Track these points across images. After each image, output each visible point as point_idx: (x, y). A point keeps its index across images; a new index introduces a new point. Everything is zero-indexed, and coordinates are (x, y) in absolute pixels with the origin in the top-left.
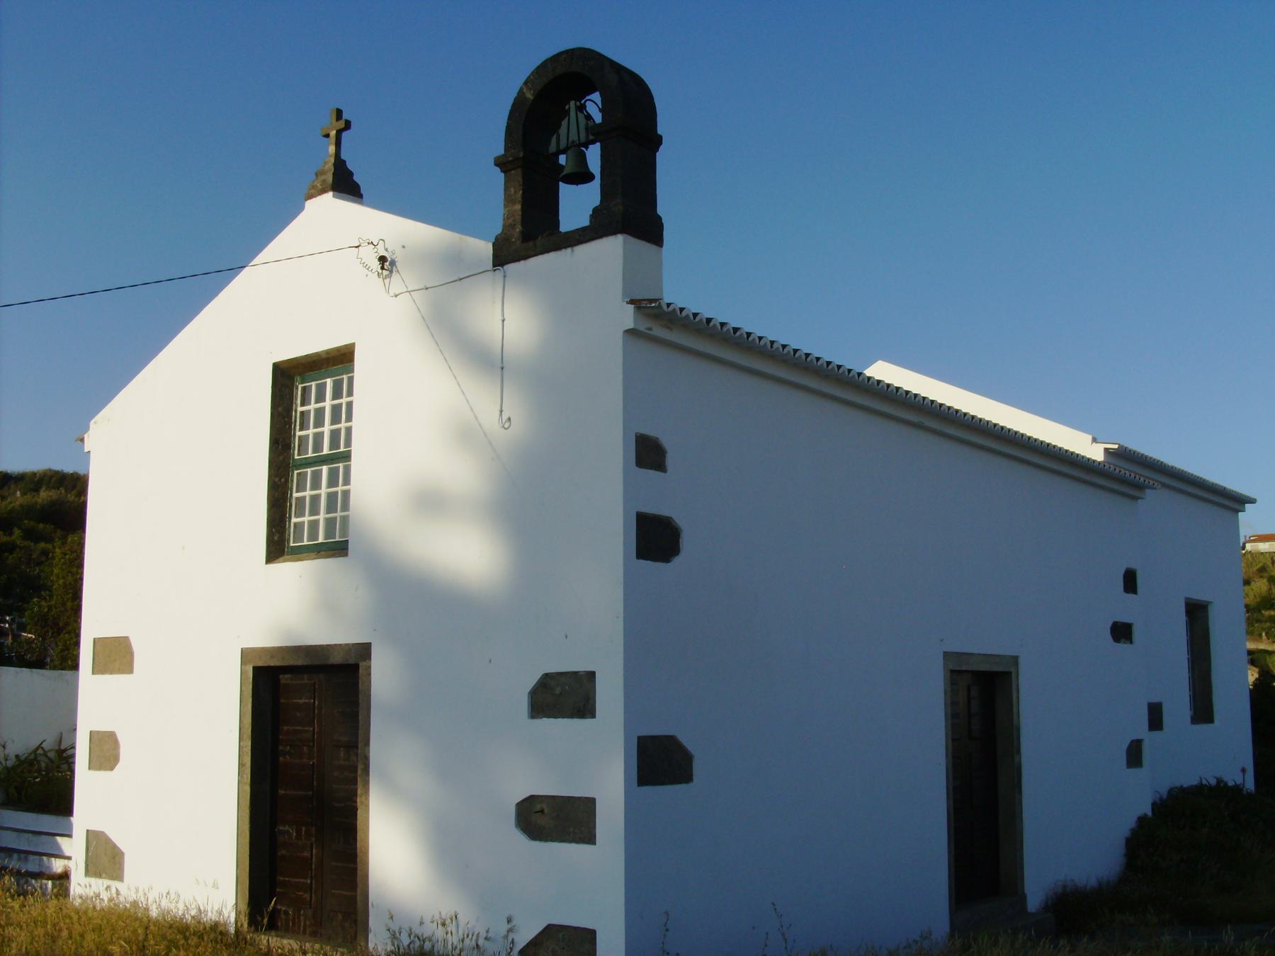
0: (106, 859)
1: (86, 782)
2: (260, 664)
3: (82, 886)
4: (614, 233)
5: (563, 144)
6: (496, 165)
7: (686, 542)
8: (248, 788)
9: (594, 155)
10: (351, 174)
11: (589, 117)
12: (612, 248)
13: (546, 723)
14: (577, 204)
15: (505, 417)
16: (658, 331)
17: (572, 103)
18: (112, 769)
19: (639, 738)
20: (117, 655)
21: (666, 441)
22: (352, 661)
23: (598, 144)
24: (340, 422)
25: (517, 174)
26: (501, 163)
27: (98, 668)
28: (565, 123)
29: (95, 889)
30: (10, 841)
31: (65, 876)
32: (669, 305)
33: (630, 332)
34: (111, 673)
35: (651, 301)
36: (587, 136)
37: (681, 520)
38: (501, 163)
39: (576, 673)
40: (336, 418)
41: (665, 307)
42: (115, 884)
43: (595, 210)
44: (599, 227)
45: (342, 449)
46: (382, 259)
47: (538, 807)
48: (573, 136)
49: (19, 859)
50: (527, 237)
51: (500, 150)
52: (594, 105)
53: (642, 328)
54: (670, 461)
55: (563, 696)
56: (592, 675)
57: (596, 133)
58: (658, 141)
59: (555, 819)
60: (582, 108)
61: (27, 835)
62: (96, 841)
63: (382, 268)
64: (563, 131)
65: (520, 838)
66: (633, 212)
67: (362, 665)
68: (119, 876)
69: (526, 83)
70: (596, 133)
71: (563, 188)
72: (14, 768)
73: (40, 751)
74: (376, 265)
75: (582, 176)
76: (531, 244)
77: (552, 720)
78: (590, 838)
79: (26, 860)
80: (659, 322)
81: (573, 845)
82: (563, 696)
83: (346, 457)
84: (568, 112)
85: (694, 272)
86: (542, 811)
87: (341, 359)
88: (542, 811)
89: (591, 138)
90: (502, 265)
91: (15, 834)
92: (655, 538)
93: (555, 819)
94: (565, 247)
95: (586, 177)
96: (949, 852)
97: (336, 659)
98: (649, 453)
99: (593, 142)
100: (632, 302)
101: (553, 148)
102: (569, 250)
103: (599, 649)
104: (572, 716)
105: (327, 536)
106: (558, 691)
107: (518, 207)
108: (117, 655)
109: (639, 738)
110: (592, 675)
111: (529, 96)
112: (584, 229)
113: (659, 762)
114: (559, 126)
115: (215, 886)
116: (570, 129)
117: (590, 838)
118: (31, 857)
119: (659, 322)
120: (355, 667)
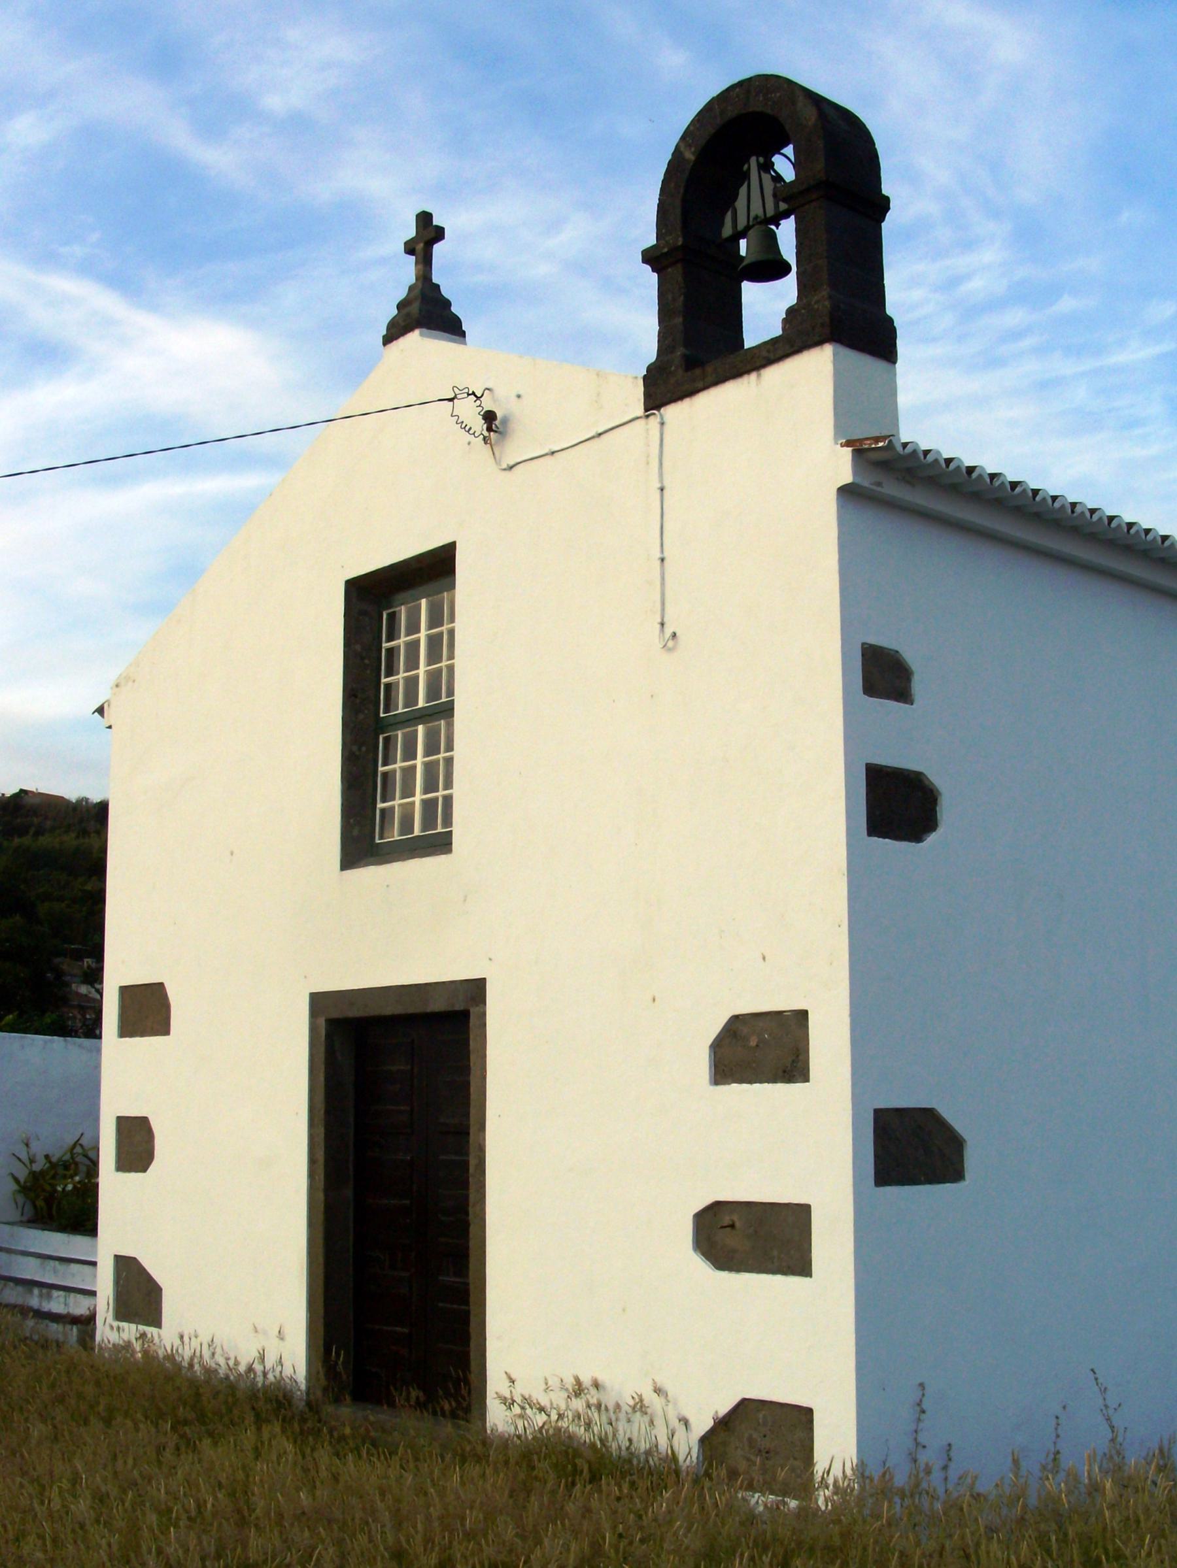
0: (139, 1293)
1: (112, 1185)
2: (335, 1014)
3: (111, 1331)
4: (819, 343)
5: (742, 223)
6: (646, 260)
7: (947, 811)
8: (321, 1196)
9: (786, 234)
10: (447, 304)
11: (778, 178)
12: (817, 367)
13: (736, 1091)
14: (765, 306)
15: (668, 632)
16: (893, 489)
17: (753, 160)
18: (144, 1170)
19: (877, 1112)
20: (148, 1010)
21: (911, 657)
22: (459, 1007)
23: (792, 220)
24: (440, 661)
25: (676, 272)
26: (650, 257)
27: (127, 1029)
28: (743, 191)
29: (125, 1336)
30: (29, 1270)
31: (88, 1321)
32: (905, 445)
33: (846, 492)
34: (142, 1035)
35: (877, 439)
36: (776, 206)
37: (937, 777)
38: (650, 257)
39: (779, 1013)
40: (434, 654)
41: (899, 449)
42: (150, 1330)
43: (791, 311)
44: (795, 338)
45: (444, 700)
46: (489, 417)
47: (726, 1221)
48: (757, 210)
49: (41, 1296)
50: (691, 363)
51: (651, 240)
52: (784, 167)
53: (866, 484)
54: (918, 686)
55: (759, 1049)
56: (803, 1015)
57: (791, 200)
58: (883, 205)
59: (752, 1237)
60: (768, 166)
61: (52, 1263)
62: (128, 1268)
63: (489, 429)
64: (741, 203)
65: (700, 1266)
66: (851, 315)
67: (474, 1011)
68: (157, 1323)
69: (683, 138)
70: (791, 200)
71: (746, 286)
72: (42, 1173)
73: (78, 1150)
74: (479, 425)
75: (770, 268)
76: (698, 371)
77: (745, 1086)
78: (802, 1267)
79: (49, 1297)
80: (896, 484)
81: (779, 1279)
82: (759, 1049)
83: (447, 711)
84: (746, 176)
85: (945, 404)
86: (732, 1226)
87: (434, 569)
88: (732, 1226)
89: (783, 206)
90: (658, 407)
91: (38, 1261)
92: (896, 804)
93: (752, 1237)
94: (748, 372)
95: (777, 269)
96: (482, 1149)
97: (437, 1005)
98: (882, 674)
99: (786, 215)
100: (848, 444)
101: (727, 231)
102: (753, 376)
103: (816, 982)
104: (774, 1080)
105: (425, 827)
106: (753, 1042)
107: (679, 320)
108: (148, 1010)
109: (877, 1112)
110: (803, 1015)
111: (690, 156)
112: (774, 341)
113: (909, 1148)
114: (735, 197)
115: (281, 1335)
116: (751, 200)
117: (802, 1267)
118: (55, 1293)
119: (896, 484)
120: (464, 1015)
